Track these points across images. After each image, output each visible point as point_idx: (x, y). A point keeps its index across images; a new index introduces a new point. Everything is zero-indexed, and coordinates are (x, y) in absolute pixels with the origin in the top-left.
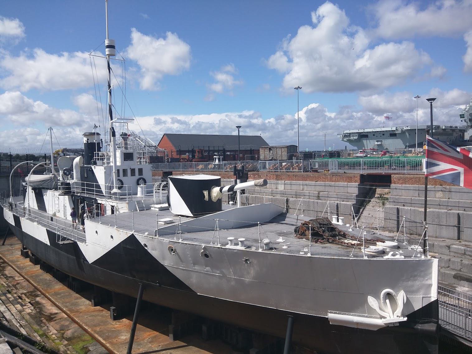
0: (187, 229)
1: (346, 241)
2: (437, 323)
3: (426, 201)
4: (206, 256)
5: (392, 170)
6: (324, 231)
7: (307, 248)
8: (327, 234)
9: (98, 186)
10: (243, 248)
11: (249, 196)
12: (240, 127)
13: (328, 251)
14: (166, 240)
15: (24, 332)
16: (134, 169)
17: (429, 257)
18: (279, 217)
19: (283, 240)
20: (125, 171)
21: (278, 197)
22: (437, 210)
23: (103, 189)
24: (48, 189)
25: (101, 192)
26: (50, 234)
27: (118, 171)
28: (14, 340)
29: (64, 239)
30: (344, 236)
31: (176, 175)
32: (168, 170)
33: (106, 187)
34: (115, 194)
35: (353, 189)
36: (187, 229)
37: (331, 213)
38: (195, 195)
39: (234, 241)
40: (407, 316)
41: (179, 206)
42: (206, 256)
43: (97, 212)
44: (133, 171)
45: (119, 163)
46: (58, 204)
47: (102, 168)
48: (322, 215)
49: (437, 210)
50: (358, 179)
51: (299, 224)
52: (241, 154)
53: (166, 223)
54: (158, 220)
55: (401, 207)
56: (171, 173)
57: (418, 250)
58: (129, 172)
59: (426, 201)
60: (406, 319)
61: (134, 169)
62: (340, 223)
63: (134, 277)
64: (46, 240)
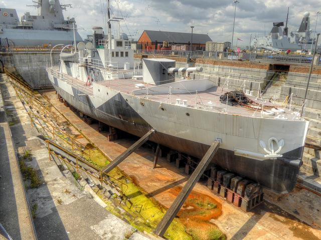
0: (153, 93)
1: (252, 106)
2: (301, 160)
3: (308, 84)
4: (163, 109)
5: (122, 55)
6: (239, 99)
7: (228, 110)
8: (240, 101)
9: (101, 62)
10: (185, 106)
11: (242, 82)
12: (193, 27)
13: (239, 111)
14: (139, 97)
15: (57, 143)
16: (118, 52)
17: (304, 120)
18: (210, 89)
19: (211, 104)
20: (117, 53)
21: (214, 76)
22: (316, 91)
23: (104, 64)
24: (73, 62)
25: (103, 66)
26: (74, 89)
27: (113, 53)
28: (51, 147)
29: (81, 93)
30: (252, 102)
31: (150, 58)
32: (145, 55)
33: (106, 63)
34: (110, 67)
35: (263, 74)
36: (153, 93)
37: (247, 88)
38: (163, 74)
39: (181, 102)
40: (283, 154)
41: (148, 78)
42: (163, 109)
43: (99, 79)
44: (122, 53)
45: (113, 48)
46: (78, 73)
47: (103, 50)
48: (239, 89)
49: (316, 91)
50: (268, 67)
51: (223, 94)
52: (196, 47)
53: (140, 87)
54: (138, 86)
55: (293, 87)
56: (146, 57)
57: (297, 115)
58: (120, 54)
59: (308, 84)
60: (282, 156)
61: (118, 52)
62: (250, 95)
63: (120, 118)
64: (71, 92)
